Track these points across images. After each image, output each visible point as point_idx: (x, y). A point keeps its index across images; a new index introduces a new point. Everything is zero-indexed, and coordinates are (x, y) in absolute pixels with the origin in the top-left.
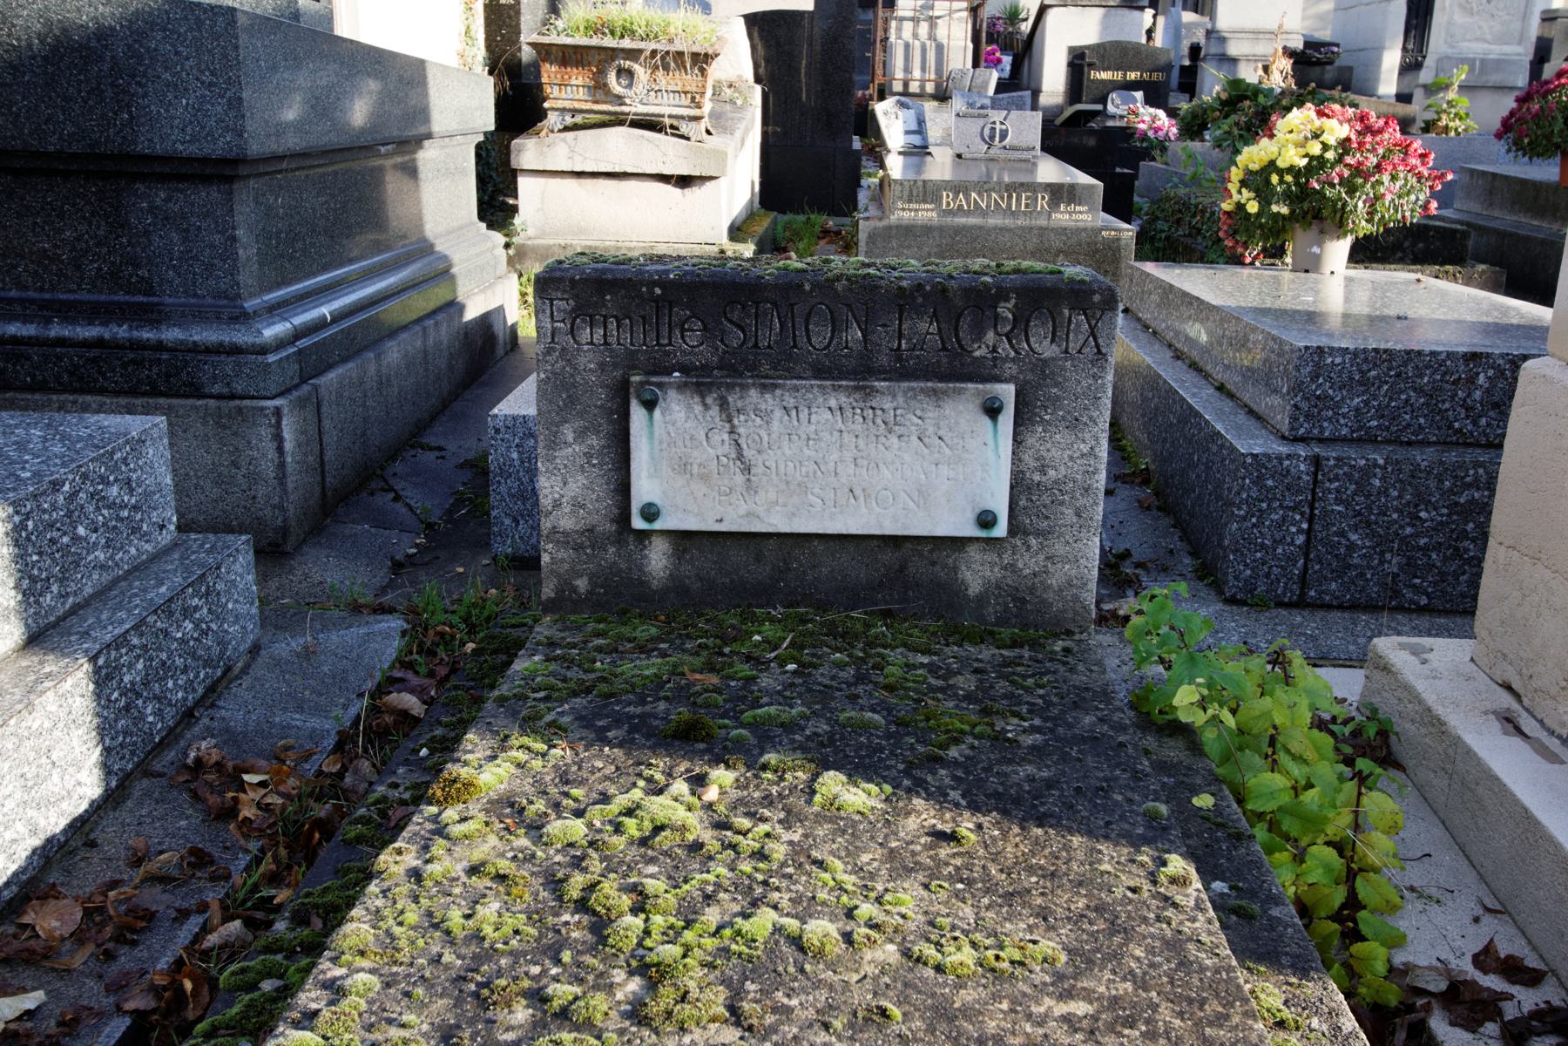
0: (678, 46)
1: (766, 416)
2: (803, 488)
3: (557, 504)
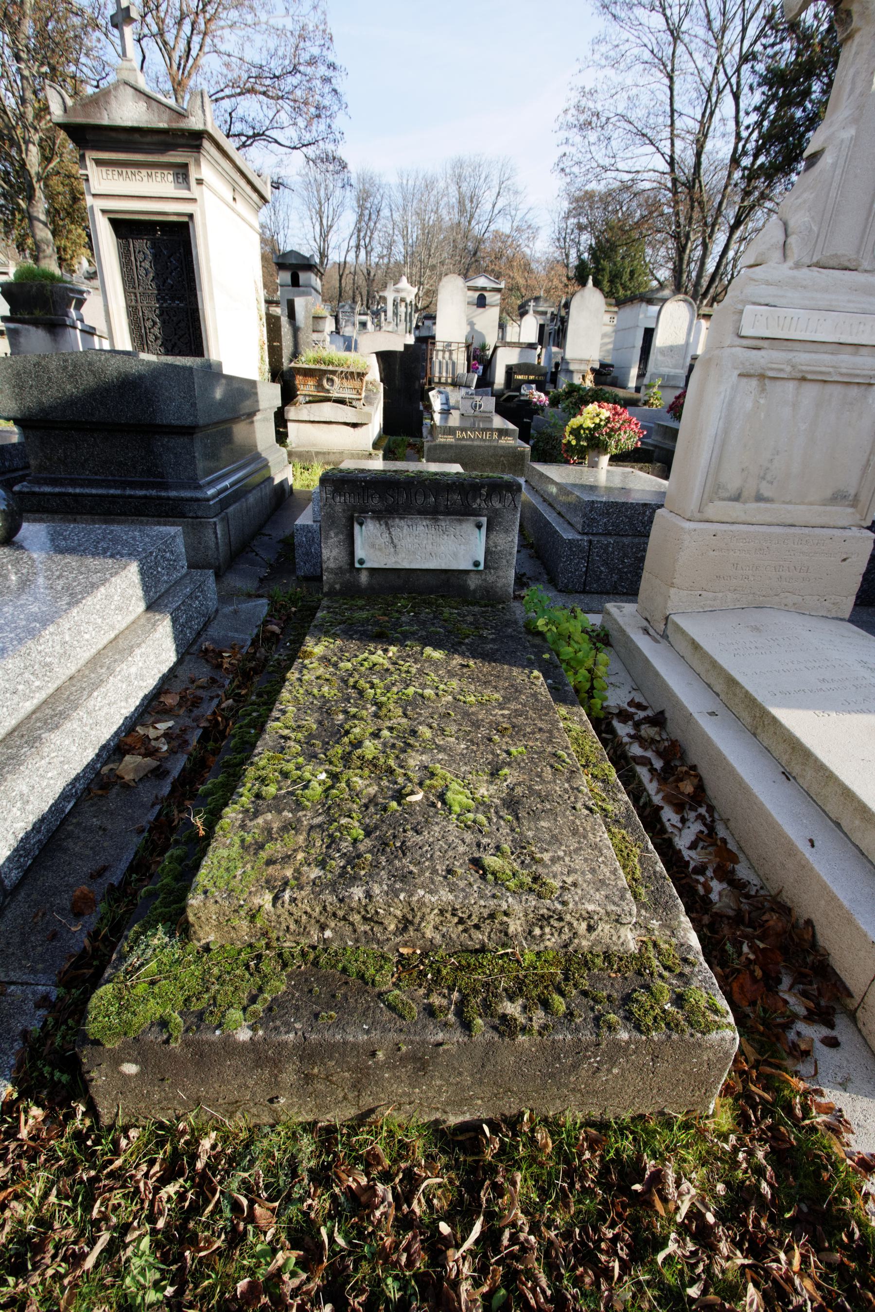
0: (351, 369)
1: (401, 528)
2: (414, 553)
3: (328, 559)
